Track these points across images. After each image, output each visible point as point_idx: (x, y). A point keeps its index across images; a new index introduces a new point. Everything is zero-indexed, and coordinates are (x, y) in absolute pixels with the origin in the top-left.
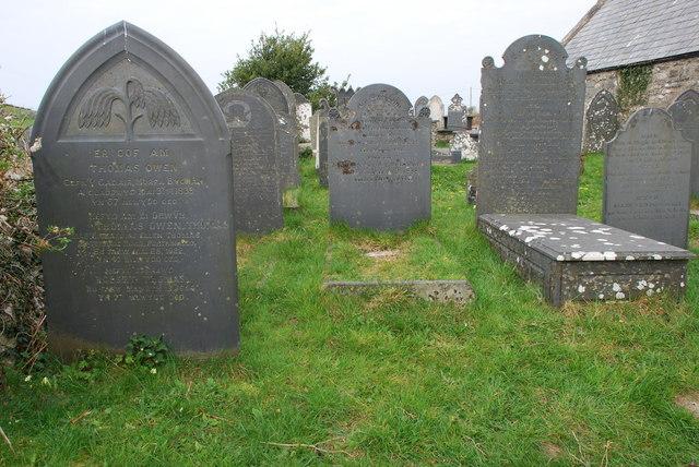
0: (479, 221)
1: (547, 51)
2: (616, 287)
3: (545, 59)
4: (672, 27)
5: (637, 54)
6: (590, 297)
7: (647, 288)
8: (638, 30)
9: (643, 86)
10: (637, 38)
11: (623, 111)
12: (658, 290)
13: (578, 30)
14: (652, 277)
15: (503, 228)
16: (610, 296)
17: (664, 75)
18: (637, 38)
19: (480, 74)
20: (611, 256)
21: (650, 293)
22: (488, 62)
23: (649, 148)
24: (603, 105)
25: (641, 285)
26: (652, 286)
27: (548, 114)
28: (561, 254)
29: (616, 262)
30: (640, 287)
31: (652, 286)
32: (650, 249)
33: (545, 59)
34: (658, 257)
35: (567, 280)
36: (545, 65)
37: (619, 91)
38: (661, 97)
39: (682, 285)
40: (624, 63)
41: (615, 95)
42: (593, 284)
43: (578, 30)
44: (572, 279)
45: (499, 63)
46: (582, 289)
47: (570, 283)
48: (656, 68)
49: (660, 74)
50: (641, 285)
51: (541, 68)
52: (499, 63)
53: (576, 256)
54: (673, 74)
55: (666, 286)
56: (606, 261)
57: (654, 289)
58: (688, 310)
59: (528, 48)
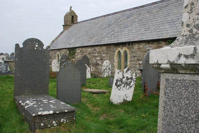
0: (14, 99)
1: (37, 43)
2: (54, 122)
3: (37, 46)
4: (81, 39)
5: (72, 45)
6: (45, 127)
7: (64, 121)
8: (73, 39)
9: (74, 54)
10: (72, 41)
11: (70, 60)
12: (67, 121)
13: (58, 37)
14: (65, 117)
15: (20, 102)
16: (52, 125)
17: (79, 51)
18: (72, 41)
19: (15, 49)
20: (51, 112)
21: (65, 122)
22: (17, 45)
23: (69, 73)
24: (64, 58)
25: (62, 120)
26: (65, 120)
27: (38, 63)
28: (34, 113)
29: (53, 114)
30: (62, 121)
31: (65, 120)
32: (64, 109)
33: (37, 46)
34: (66, 111)
35: (37, 122)
36: (37, 47)
37: (68, 54)
38: (78, 57)
39: (74, 119)
40: (69, 47)
41: (67, 55)
42: (46, 122)
43: (58, 37)
44: (38, 121)
45: (21, 46)
46: (42, 124)
47: (38, 123)
48: (77, 49)
49: (78, 51)
50: (62, 120)
51: (36, 48)
52: (21, 46)
53: (39, 113)
54: (81, 51)
55: (70, 120)
56: (50, 114)
57: (66, 121)
58: (76, 127)
59: (32, 43)
